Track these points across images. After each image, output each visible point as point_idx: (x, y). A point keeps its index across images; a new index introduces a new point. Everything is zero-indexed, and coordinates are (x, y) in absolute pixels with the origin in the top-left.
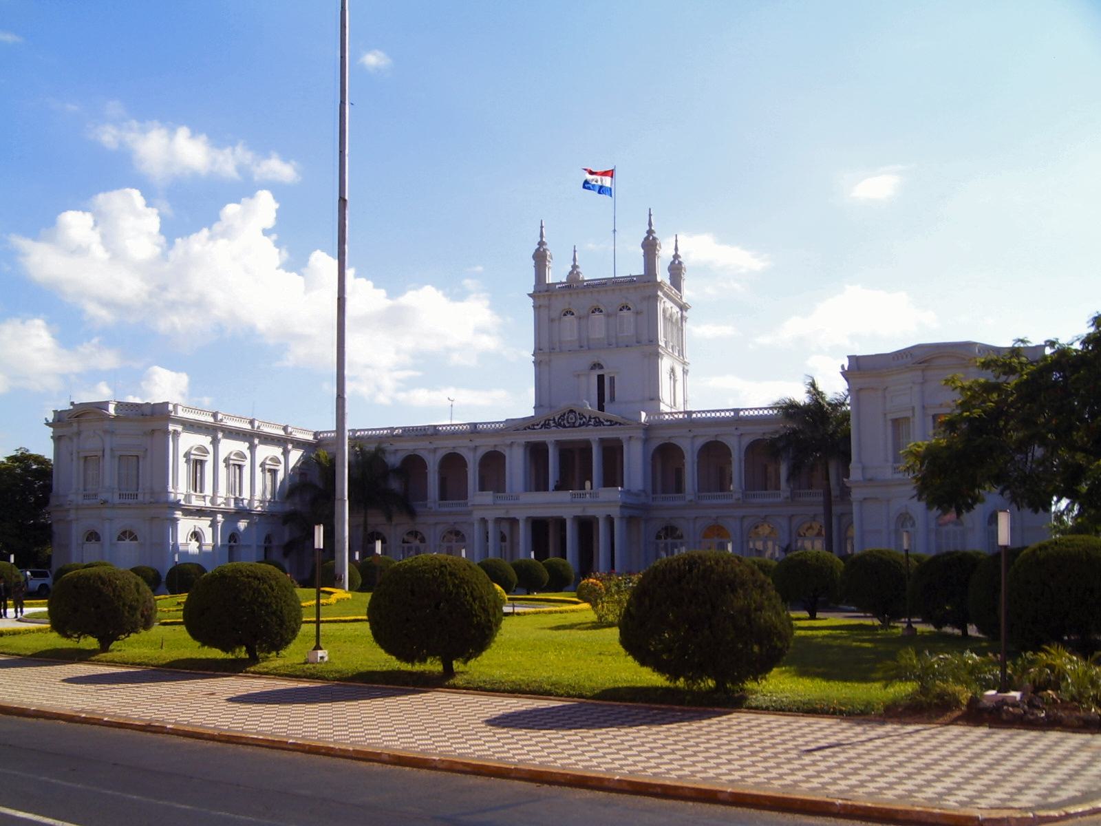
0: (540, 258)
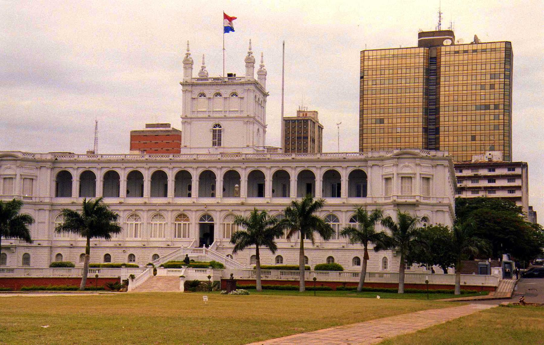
0: (188, 63)
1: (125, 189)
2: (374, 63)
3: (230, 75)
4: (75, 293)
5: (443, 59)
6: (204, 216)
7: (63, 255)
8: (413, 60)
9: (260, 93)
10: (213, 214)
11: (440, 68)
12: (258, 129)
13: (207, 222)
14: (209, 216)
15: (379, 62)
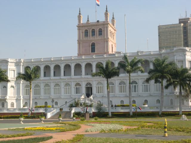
1: (53, 71)
2: (163, 30)
3: (98, 21)
4: (171, 112)
5: (188, 27)
6: (88, 84)
7: (38, 102)
8: (177, 28)
9: (112, 29)
10: (91, 83)
11: (188, 34)
12: (112, 45)
13: (89, 86)
14: (90, 83)
15: (165, 30)
